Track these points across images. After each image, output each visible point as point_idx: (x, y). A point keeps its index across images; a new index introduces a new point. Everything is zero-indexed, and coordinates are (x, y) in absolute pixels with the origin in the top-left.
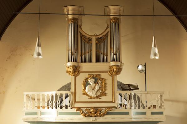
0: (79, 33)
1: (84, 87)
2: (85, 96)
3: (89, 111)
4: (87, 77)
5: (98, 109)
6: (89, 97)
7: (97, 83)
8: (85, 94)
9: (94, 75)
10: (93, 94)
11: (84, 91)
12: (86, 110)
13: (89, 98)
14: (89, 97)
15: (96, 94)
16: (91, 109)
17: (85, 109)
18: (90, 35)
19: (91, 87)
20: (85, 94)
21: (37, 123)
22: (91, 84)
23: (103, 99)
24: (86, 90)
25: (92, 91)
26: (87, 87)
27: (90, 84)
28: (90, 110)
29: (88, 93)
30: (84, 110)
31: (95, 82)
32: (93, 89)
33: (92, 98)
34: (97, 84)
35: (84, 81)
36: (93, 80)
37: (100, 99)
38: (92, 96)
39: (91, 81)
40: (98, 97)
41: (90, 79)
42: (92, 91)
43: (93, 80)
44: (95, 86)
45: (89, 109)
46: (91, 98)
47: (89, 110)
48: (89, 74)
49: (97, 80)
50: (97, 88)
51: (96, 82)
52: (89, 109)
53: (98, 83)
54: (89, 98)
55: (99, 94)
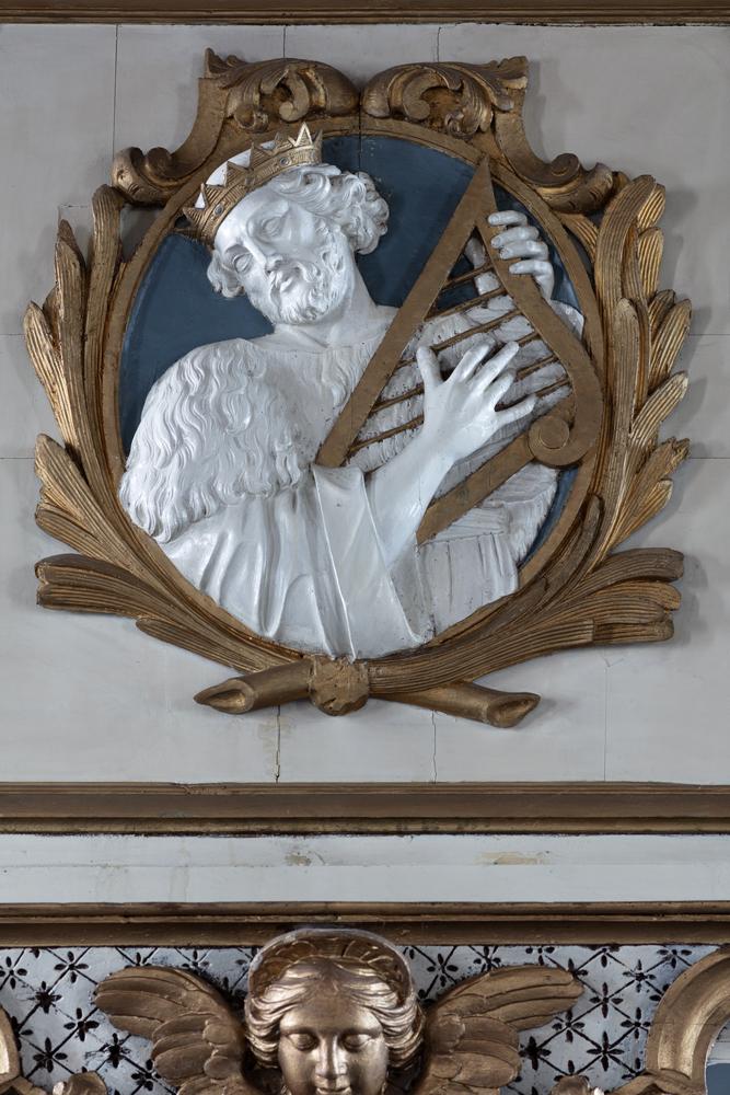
0: (279, 1016)
1: (89, 406)
2: (117, 632)
3: (215, 1029)
4: (165, 130)
5: (450, 982)
6: (213, 674)
7: (435, 277)
8: (106, 576)
9: (354, 90)
10: (368, 562)
11: (79, 507)
12: (116, 1000)
13: (213, 698)
14: (213, 674)
15: (409, 580)
16: (267, 976)
17: (104, 961)
18: (183, 977)
19: (284, 387)
20: (106, 576)
21: (496, 383)
22: (288, 303)
23: (610, 712)
24: (147, 484)
25: (304, 496)
26: (163, 404)
27: (248, 321)
28: (232, 1000)
29: (188, 556)
30: (72, 998)
31: (384, 274)
32: (344, 446)
33: (302, 697)
34: (442, 306)
35: (87, 219)
36: (356, 203)
37: (513, 709)
38: (314, 635)
39: (290, 241)
40: (452, 668)
41: (246, 182)
42: (304, 496)
43: (356, 203)
44: (390, 360)
45: (222, 961)
46: (276, 681)
47: (199, 999)
48: (215, 63)
49: (445, 203)
50: (468, 411)
51: (411, 269)
52: (222, 961)
53: (457, 294)
54: (213, 698)
55: (486, 568)
